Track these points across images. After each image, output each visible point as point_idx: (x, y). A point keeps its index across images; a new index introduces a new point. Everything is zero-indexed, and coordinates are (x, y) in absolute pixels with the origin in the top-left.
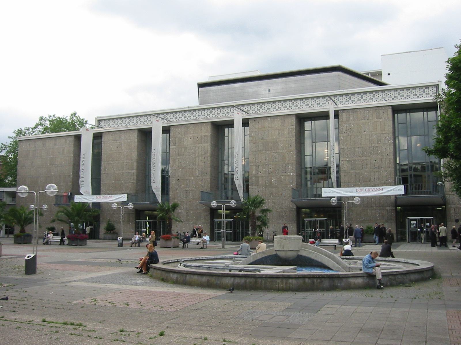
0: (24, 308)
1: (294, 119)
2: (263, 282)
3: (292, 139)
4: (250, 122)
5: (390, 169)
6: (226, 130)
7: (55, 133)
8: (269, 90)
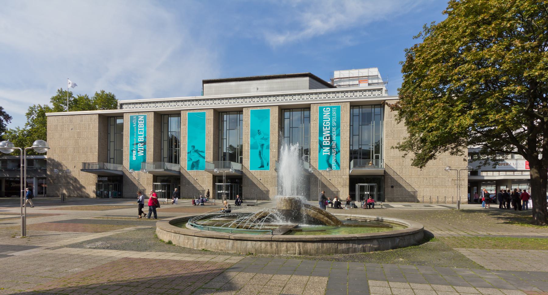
0: (53, 260)
1: (213, 111)
2: (196, 242)
3: (275, 124)
4: (244, 110)
5: (346, 149)
6: (225, 116)
7: (90, 110)
8: (258, 89)
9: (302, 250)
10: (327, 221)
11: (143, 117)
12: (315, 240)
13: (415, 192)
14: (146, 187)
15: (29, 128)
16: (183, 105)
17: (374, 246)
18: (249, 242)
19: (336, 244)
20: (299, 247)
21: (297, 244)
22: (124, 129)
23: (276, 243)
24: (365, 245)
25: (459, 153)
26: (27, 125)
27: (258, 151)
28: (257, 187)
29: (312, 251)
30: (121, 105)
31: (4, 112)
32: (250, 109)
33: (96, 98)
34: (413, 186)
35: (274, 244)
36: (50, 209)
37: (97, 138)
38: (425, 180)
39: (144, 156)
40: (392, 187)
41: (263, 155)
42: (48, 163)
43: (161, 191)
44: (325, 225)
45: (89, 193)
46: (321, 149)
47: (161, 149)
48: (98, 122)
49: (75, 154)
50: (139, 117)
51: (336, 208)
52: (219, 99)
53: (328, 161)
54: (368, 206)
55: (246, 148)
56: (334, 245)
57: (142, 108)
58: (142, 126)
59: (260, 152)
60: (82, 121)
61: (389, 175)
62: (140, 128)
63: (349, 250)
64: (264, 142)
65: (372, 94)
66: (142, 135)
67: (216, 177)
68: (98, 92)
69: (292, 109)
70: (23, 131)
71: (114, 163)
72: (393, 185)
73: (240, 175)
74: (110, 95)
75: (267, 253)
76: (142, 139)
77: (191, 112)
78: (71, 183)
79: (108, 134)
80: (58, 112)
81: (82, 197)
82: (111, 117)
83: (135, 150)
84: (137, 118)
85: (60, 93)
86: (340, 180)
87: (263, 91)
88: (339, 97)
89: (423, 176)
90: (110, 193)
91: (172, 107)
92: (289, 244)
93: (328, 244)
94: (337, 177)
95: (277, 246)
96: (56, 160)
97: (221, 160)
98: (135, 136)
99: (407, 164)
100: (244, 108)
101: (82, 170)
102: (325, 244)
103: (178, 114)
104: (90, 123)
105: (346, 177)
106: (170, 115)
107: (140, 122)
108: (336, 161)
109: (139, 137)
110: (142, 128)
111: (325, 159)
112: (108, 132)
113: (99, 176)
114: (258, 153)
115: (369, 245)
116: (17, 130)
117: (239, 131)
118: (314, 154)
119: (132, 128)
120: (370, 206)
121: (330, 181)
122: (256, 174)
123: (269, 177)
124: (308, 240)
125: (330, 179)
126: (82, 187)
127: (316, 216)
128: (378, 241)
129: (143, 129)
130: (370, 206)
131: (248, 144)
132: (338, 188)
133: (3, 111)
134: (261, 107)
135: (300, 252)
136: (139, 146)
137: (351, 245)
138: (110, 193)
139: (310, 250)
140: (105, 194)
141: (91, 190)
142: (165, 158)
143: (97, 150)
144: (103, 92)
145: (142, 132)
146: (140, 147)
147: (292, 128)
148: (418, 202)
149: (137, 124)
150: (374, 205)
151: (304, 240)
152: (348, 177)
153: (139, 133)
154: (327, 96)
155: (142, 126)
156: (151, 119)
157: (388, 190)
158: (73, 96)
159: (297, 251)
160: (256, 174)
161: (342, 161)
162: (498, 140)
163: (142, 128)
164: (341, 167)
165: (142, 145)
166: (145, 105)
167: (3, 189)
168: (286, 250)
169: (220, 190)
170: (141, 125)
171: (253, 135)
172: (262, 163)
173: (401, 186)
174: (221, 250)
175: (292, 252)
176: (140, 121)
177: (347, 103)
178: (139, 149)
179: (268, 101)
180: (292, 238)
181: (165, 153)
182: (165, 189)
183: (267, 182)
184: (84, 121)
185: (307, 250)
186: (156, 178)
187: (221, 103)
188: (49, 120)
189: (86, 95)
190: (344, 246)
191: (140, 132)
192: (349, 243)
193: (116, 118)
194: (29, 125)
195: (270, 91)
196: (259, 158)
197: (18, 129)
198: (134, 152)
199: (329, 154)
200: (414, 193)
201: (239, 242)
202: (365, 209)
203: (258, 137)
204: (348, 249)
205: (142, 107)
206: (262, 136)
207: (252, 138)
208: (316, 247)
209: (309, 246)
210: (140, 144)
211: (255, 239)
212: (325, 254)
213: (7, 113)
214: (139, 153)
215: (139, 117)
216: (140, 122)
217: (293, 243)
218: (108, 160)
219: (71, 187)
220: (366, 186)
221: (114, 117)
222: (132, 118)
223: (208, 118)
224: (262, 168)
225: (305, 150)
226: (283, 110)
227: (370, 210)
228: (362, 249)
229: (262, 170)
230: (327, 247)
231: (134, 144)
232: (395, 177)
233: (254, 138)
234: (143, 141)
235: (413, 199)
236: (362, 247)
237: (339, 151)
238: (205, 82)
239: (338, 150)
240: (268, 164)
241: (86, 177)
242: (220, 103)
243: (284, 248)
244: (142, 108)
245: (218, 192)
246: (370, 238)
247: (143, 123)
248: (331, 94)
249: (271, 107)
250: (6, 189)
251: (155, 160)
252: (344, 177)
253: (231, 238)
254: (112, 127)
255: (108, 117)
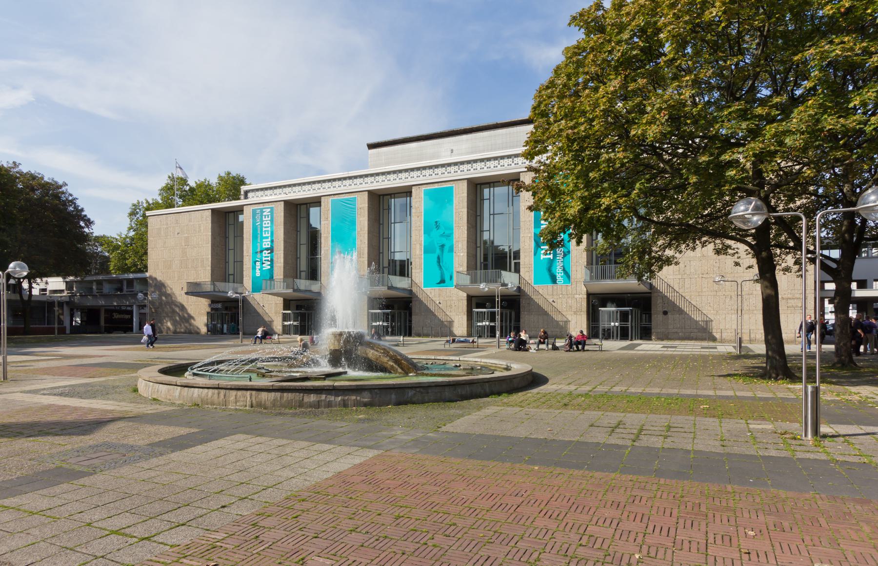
3: (463, 210)
4: (413, 190)
8: (452, 151)
9: (254, 402)
10: (392, 366)
11: (269, 210)
12: (271, 388)
13: (708, 322)
14: (274, 318)
15: (132, 233)
16: (396, 179)
17: (362, 400)
18: (197, 389)
19: (302, 394)
20: (251, 398)
21: (249, 393)
22: (244, 230)
23: (225, 391)
24: (346, 398)
25: (730, 251)
26: (130, 229)
27: (436, 256)
28: (435, 315)
29: (267, 403)
30: (246, 193)
31: (85, 216)
32: (423, 188)
33: (219, 183)
34: (704, 312)
35: (222, 392)
36: (116, 350)
37: (210, 245)
38: (728, 300)
39: (271, 270)
40: (665, 313)
41: (444, 263)
42: (150, 284)
43: (381, 323)
44: (390, 372)
45: (200, 327)
46: (537, 249)
47: (297, 258)
48: (210, 222)
49: (182, 270)
50: (264, 210)
51: (517, 350)
52: (406, 170)
53: (549, 270)
54: (575, 346)
55: (418, 252)
56: (297, 396)
57: (375, 184)
58: (268, 223)
59: (439, 258)
60: (190, 221)
61: (658, 291)
62: (265, 227)
63: (320, 403)
64: (444, 241)
65: (485, 166)
66: (267, 238)
67: (473, 298)
68: (221, 175)
69: (494, 182)
70: (125, 239)
71: (234, 282)
72: (665, 310)
73: (408, 296)
74: (238, 178)
75: (214, 405)
76: (268, 245)
77: (336, 198)
78: (177, 313)
79: (297, 231)
80: (166, 208)
81: (190, 333)
82: (301, 204)
83: (258, 261)
84: (262, 211)
85: (171, 180)
86: (570, 302)
87: (461, 154)
88: (518, 164)
89: (724, 293)
90: (225, 326)
91: (401, 181)
92: (240, 393)
93: (290, 394)
94: (566, 296)
95: (225, 396)
96: (159, 278)
97: (481, 269)
98: (259, 239)
99: (692, 271)
100: (413, 187)
101: (187, 293)
102: (285, 394)
103: (406, 192)
104: (201, 223)
105: (581, 296)
106: (393, 196)
107: (265, 218)
108: (564, 270)
109: (264, 240)
110: (268, 227)
111: (545, 266)
112: (226, 235)
113: (213, 302)
114: (436, 260)
115: (354, 398)
116: (119, 238)
117: (409, 224)
118: (526, 259)
119: (255, 228)
120: (577, 347)
121: (553, 304)
122: (433, 294)
123: (454, 298)
124: (262, 388)
125: (553, 301)
126: (191, 317)
127: (377, 359)
128: (371, 393)
129: (269, 229)
130: (577, 347)
131: (421, 245)
132: (567, 316)
133: (83, 213)
134: (440, 184)
135: (252, 404)
136: (264, 255)
137: (323, 397)
138: (225, 326)
139: (265, 401)
140: (219, 329)
141: (201, 322)
142: (303, 271)
143: (210, 264)
144: (229, 173)
145: (268, 234)
146: (266, 257)
147: (494, 214)
148: (714, 339)
149: (262, 221)
150: (584, 344)
151: (256, 387)
152: (585, 296)
153: (264, 235)
154: (459, 169)
155: (268, 223)
156: (280, 209)
157: (657, 318)
158: (188, 183)
159: (248, 403)
160: (433, 294)
161: (574, 269)
162: (682, 229)
163: (268, 227)
164: (572, 280)
165: (268, 253)
166: (439, 171)
167: (102, 323)
168: (234, 400)
169: (376, 322)
170: (267, 222)
171: (427, 231)
172: (442, 275)
173: (681, 311)
174: (170, 400)
175: (241, 403)
176: (265, 216)
177: (364, 193)
178: (264, 259)
179: (513, 164)
180: (242, 385)
181: (303, 265)
182: (387, 321)
183: (451, 306)
184: (193, 221)
185: (261, 402)
186: (287, 304)
187: (398, 179)
188: (150, 221)
189: (205, 180)
190: (313, 398)
191: (265, 234)
192: (321, 393)
193: (308, 205)
194: (132, 230)
195: (472, 153)
196: (437, 268)
197: (120, 235)
198: (258, 264)
199: (551, 256)
200: (707, 324)
201: (186, 389)
202: (567, 351)
203: (435, 233)
204: (319, 401)
205: (386, 180)
206: (441, 231)
207: (427, 235)
208: (272, 398)
209: (264, 395)
210: (266, 251)
211: (201, 386)
212: (286, 407)
213: (88, 217)
214: (264, 265)
215: (264, 210)
216: (265, 218)
217: (244, 392)
218: (225, 279)
219: (178, 318)
220: (485, 312)
221: (306, 204)
222: (254, 211)
223: (360, 206)
224: (442, 284)
225: (514, 253)
226: (476, 187)
227: (578, 353)
228: (342, 403)
229: (442, 288)
230: (288, 398)
231: (257, 253)
232: (669, 295)
233: (429, 235)
234: (269, 246)
235: (704, 334)
236: (341, 399)
237: (569, 252)
238: (371, 146)
239: (566, 250)
240: (451, 278)
241: (196, 303)
242: (457, 172)
243: (232, 398)
244: (375, 184)
245: (479, 324)
246: (355, 388)
247: (269, 219)
248: (506, 160)
249: (456, 182)
250: (107, 321)
251: (286, 276)
252: (577, 296)
253: (178, 384)
254: (231, 227)
255: (226, 212)
